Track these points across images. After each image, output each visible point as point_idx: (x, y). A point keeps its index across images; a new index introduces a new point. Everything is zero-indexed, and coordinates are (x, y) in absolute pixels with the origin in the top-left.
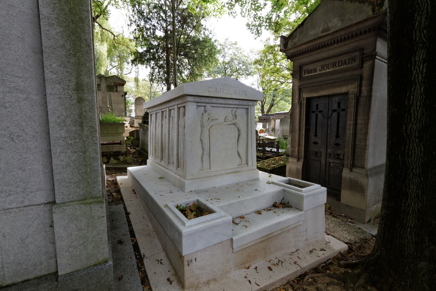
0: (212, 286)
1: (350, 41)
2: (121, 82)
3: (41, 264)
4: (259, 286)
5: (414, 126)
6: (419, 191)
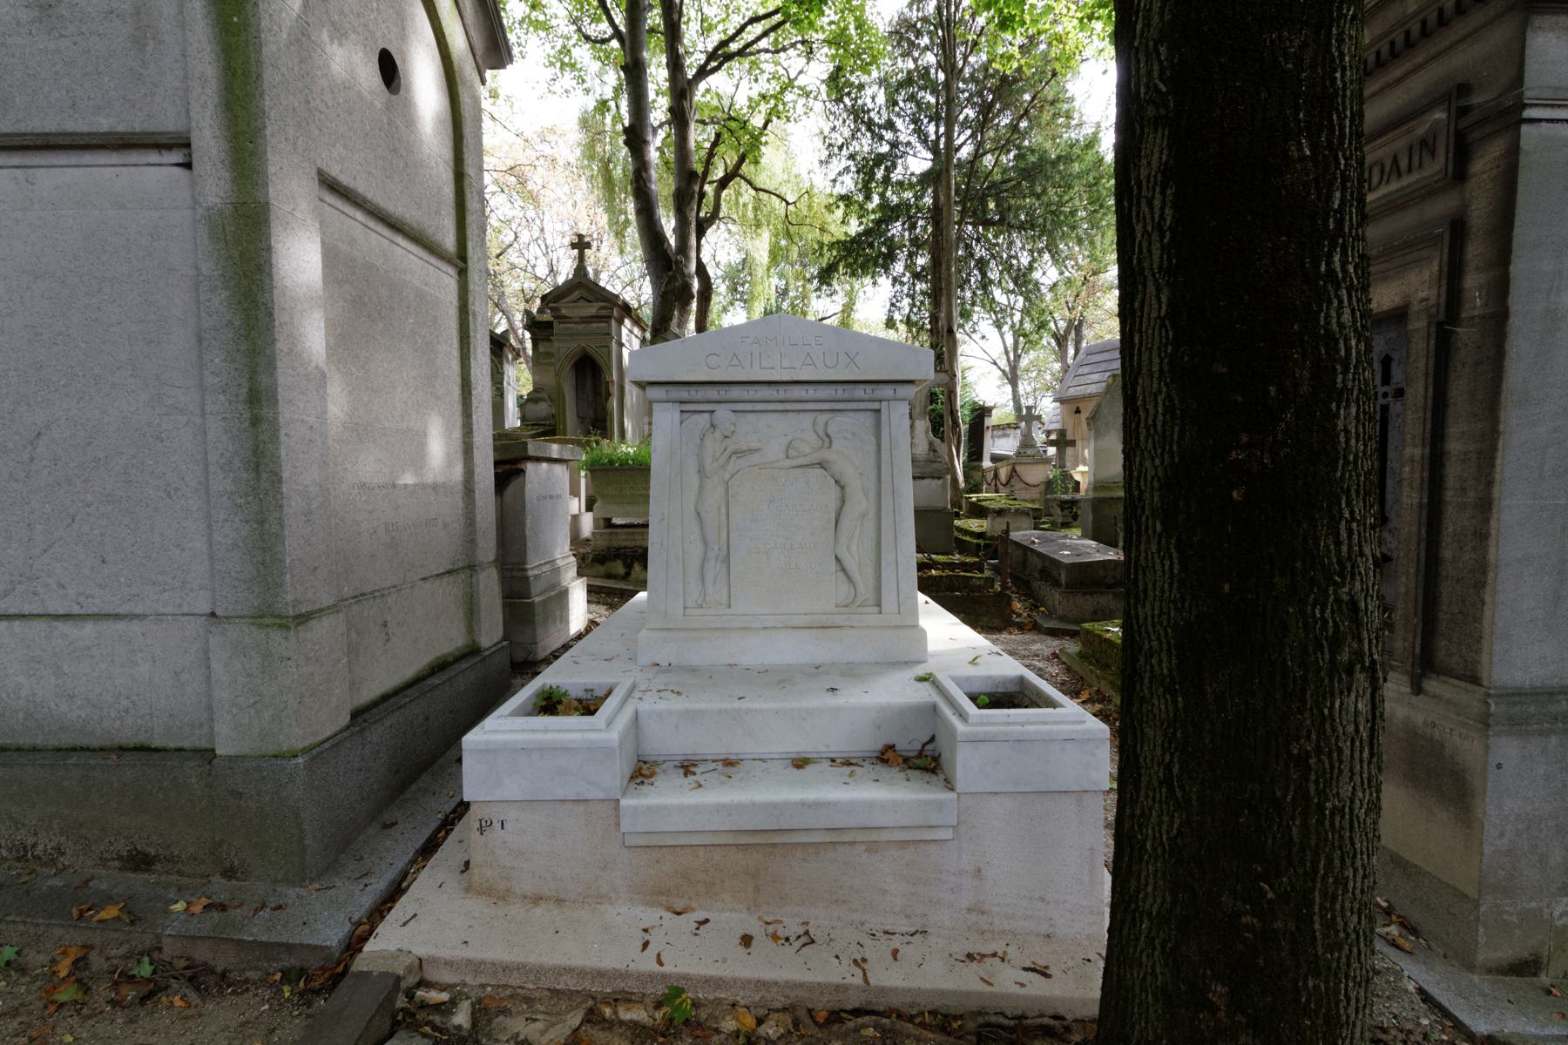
0: (538, 911)
1: (1408, 66)
3: (201, 725)
4: (661, 963)
5: (1148, 464)
6: (1172, 755)
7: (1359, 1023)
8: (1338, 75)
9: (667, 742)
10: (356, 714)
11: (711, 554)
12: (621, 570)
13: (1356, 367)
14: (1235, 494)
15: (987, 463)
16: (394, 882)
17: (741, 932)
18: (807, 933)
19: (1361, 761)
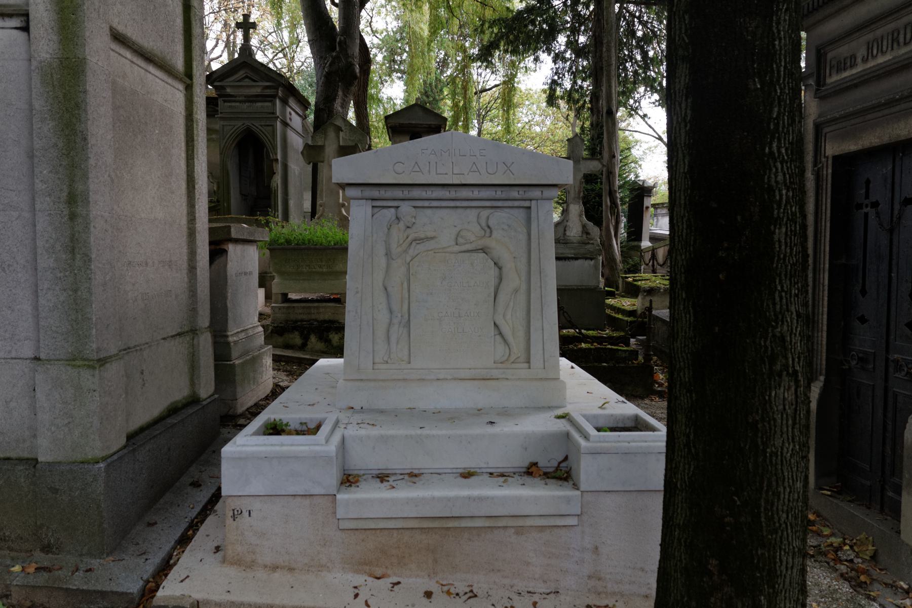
0: (276, 575)
2: (433, 122)
3: (24, 441)
7: (788, 577)
8: (777, 43)
9: (364, 459)
10: (130, 437)
11: (395, 321)
12: (297, 340)
13: (786, 205)
14: (721, 276)
15: (646, 244)
16: (163, 559)
17: (425, 590)
18: (471, 591)
19: (787, 427)
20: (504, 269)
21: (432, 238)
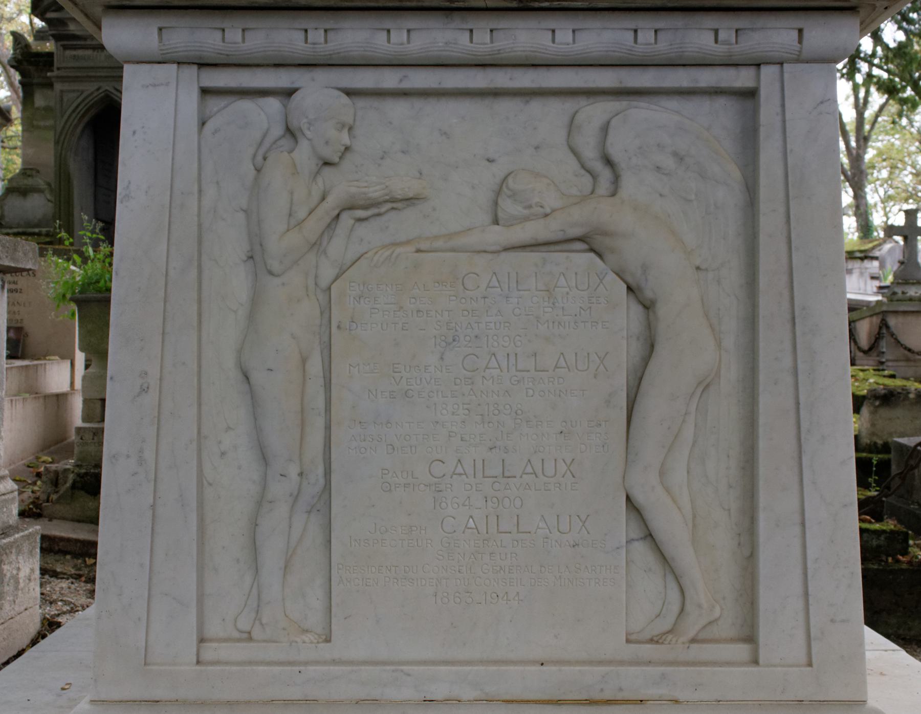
11: (279, 489)
20: (662, 310)
21: (410, 201)
